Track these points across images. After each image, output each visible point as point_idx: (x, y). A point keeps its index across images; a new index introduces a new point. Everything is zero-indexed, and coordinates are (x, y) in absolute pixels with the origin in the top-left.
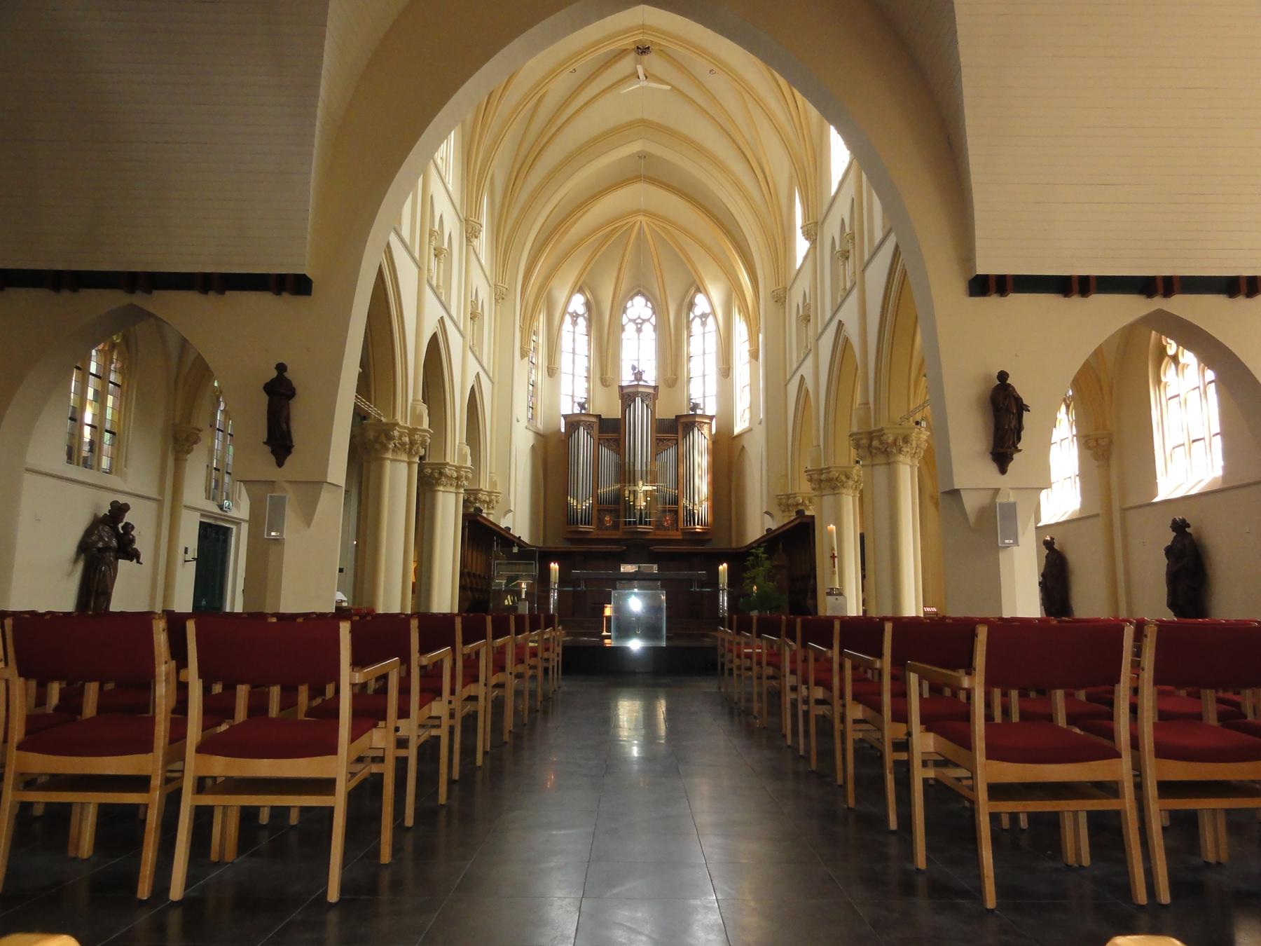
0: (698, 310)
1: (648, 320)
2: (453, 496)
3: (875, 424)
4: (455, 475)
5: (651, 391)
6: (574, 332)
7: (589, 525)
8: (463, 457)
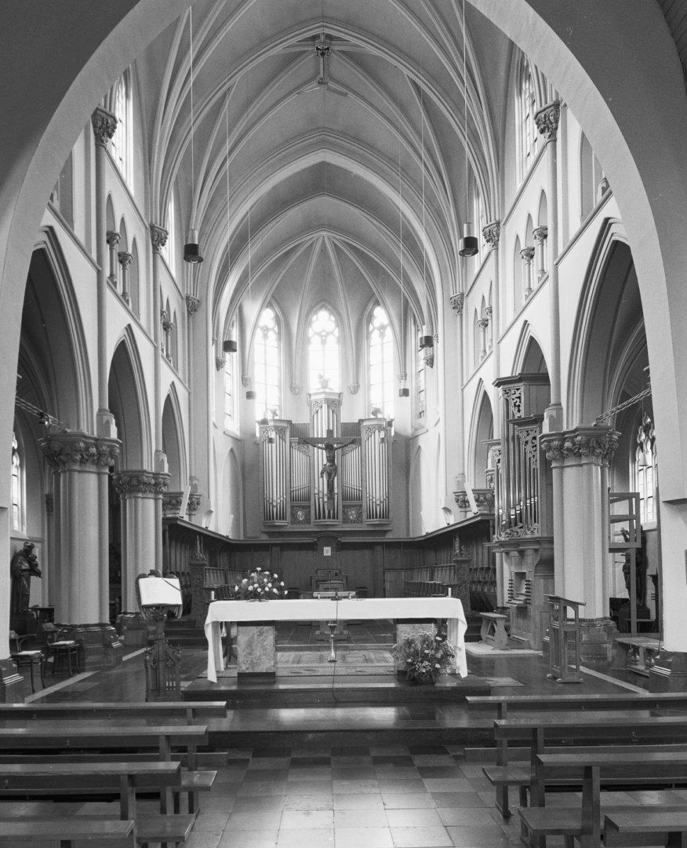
1: (332, 333)
2: (152, 502)
3: (567, 428)
4: (153, 482)
5: (337, 398)
6: (265, 345)
8: (160, 464)
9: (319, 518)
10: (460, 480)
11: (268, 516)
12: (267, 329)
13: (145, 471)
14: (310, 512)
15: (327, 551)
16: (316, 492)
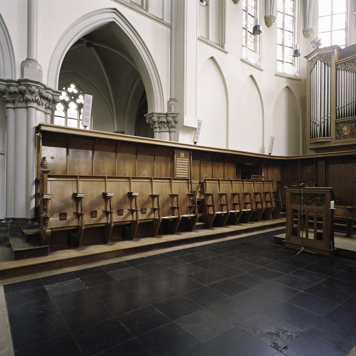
11: (313, 135)
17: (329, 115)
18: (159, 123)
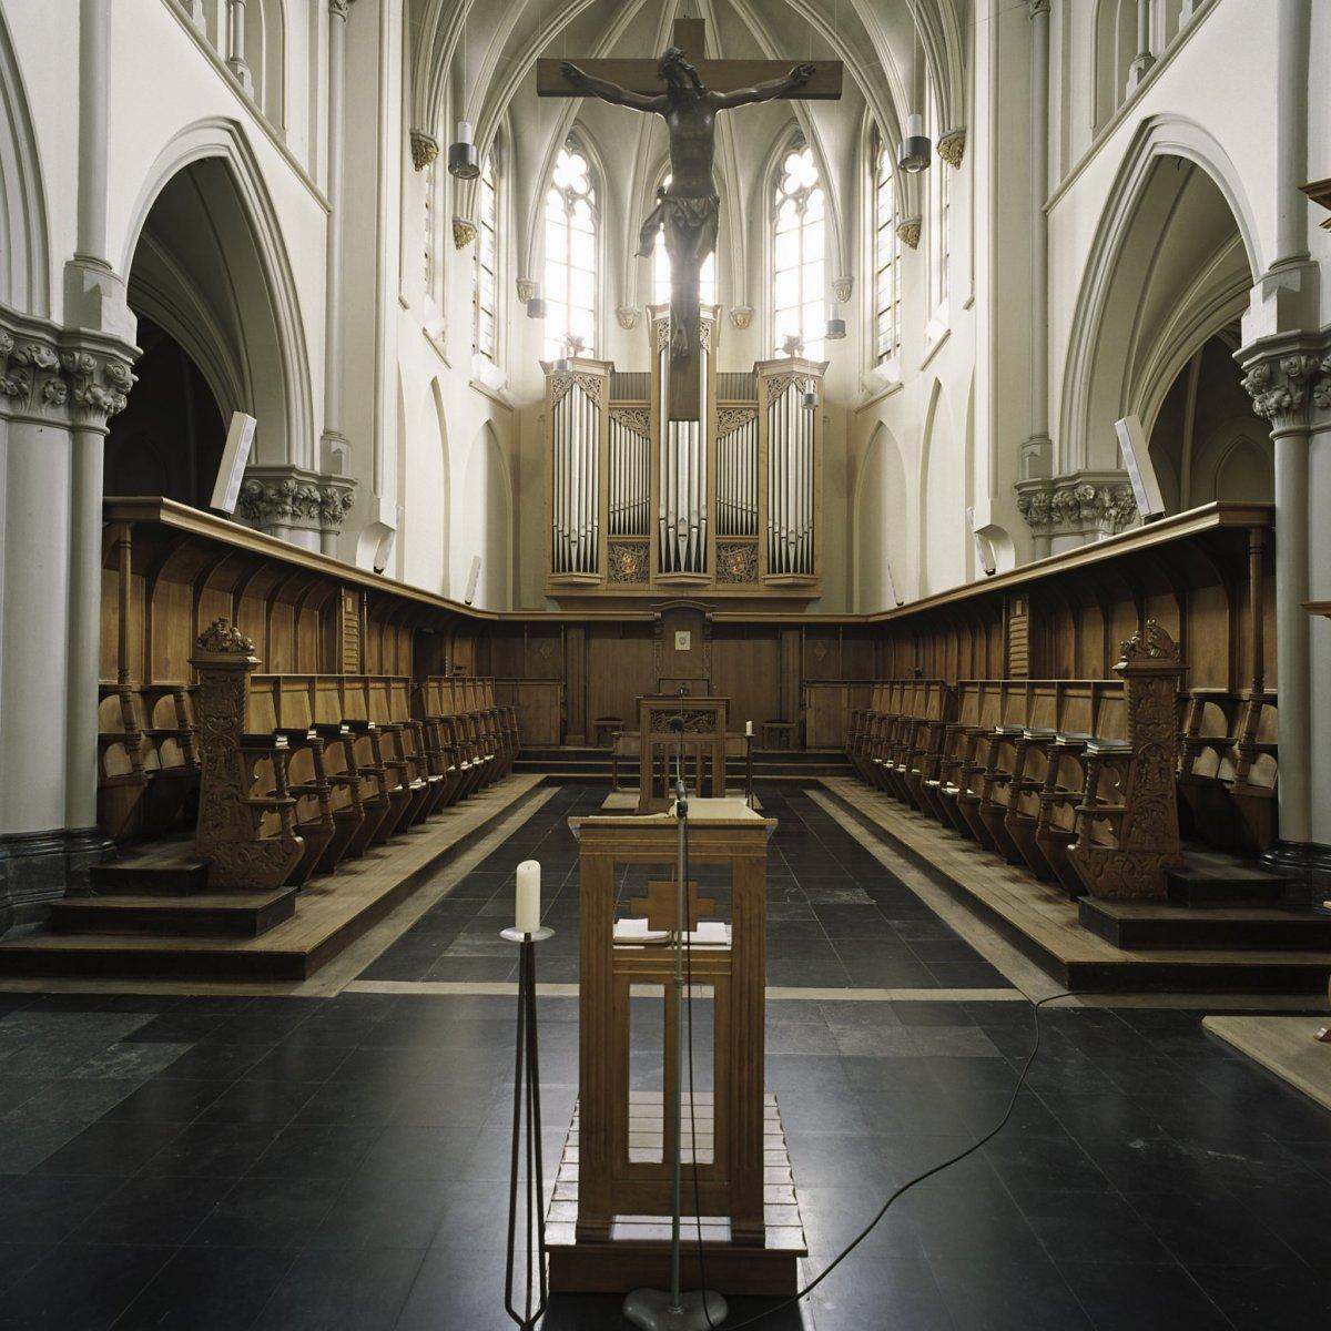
0: (790, 186)
2: (60, 441)
7: (592, 571)
9: (668, 570)
10: (1037, 449)
11: (560, 564)
12: (573, 192)
13: (292, 469)
14: (647, 556)
15: (683, 640)
16: (662, 513)
17: (596, 523)
18: (295, 499)
